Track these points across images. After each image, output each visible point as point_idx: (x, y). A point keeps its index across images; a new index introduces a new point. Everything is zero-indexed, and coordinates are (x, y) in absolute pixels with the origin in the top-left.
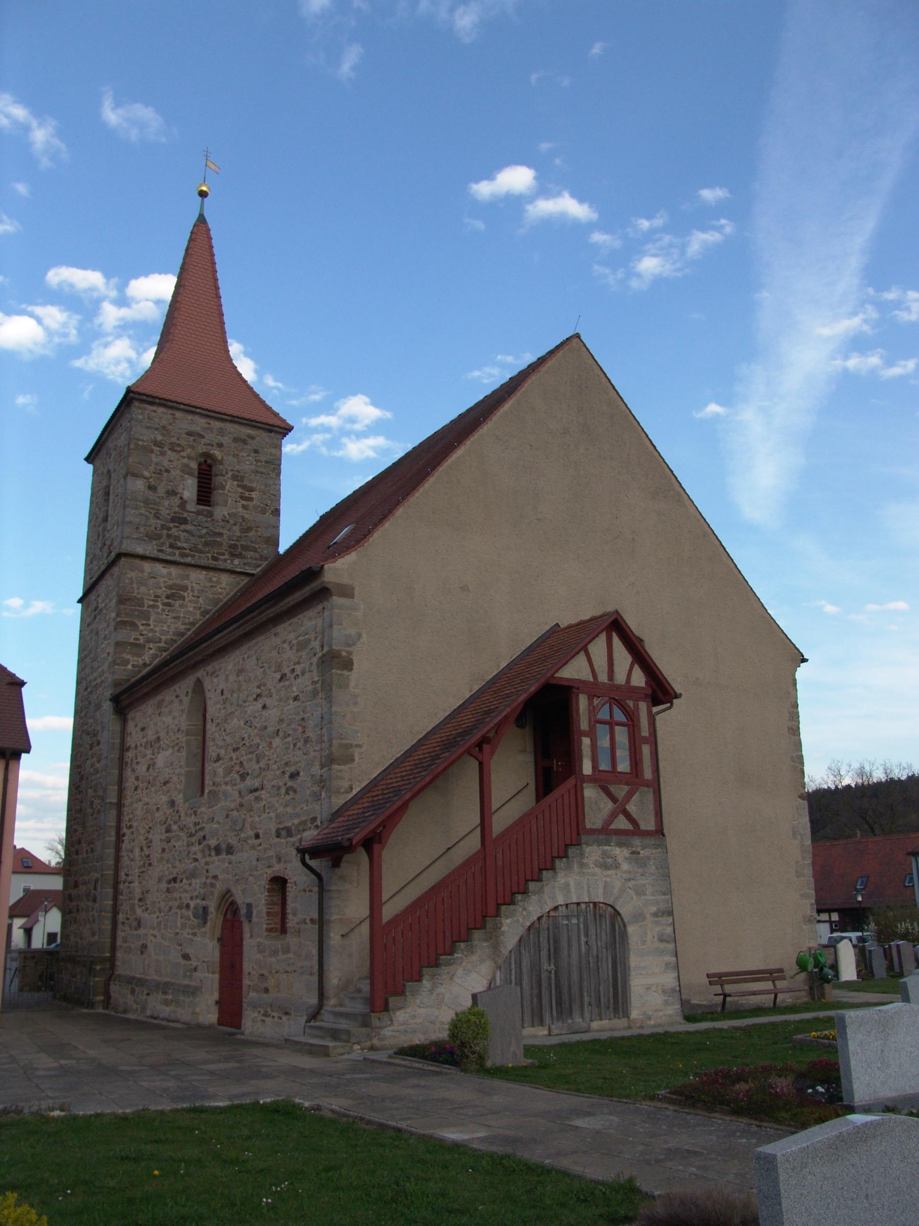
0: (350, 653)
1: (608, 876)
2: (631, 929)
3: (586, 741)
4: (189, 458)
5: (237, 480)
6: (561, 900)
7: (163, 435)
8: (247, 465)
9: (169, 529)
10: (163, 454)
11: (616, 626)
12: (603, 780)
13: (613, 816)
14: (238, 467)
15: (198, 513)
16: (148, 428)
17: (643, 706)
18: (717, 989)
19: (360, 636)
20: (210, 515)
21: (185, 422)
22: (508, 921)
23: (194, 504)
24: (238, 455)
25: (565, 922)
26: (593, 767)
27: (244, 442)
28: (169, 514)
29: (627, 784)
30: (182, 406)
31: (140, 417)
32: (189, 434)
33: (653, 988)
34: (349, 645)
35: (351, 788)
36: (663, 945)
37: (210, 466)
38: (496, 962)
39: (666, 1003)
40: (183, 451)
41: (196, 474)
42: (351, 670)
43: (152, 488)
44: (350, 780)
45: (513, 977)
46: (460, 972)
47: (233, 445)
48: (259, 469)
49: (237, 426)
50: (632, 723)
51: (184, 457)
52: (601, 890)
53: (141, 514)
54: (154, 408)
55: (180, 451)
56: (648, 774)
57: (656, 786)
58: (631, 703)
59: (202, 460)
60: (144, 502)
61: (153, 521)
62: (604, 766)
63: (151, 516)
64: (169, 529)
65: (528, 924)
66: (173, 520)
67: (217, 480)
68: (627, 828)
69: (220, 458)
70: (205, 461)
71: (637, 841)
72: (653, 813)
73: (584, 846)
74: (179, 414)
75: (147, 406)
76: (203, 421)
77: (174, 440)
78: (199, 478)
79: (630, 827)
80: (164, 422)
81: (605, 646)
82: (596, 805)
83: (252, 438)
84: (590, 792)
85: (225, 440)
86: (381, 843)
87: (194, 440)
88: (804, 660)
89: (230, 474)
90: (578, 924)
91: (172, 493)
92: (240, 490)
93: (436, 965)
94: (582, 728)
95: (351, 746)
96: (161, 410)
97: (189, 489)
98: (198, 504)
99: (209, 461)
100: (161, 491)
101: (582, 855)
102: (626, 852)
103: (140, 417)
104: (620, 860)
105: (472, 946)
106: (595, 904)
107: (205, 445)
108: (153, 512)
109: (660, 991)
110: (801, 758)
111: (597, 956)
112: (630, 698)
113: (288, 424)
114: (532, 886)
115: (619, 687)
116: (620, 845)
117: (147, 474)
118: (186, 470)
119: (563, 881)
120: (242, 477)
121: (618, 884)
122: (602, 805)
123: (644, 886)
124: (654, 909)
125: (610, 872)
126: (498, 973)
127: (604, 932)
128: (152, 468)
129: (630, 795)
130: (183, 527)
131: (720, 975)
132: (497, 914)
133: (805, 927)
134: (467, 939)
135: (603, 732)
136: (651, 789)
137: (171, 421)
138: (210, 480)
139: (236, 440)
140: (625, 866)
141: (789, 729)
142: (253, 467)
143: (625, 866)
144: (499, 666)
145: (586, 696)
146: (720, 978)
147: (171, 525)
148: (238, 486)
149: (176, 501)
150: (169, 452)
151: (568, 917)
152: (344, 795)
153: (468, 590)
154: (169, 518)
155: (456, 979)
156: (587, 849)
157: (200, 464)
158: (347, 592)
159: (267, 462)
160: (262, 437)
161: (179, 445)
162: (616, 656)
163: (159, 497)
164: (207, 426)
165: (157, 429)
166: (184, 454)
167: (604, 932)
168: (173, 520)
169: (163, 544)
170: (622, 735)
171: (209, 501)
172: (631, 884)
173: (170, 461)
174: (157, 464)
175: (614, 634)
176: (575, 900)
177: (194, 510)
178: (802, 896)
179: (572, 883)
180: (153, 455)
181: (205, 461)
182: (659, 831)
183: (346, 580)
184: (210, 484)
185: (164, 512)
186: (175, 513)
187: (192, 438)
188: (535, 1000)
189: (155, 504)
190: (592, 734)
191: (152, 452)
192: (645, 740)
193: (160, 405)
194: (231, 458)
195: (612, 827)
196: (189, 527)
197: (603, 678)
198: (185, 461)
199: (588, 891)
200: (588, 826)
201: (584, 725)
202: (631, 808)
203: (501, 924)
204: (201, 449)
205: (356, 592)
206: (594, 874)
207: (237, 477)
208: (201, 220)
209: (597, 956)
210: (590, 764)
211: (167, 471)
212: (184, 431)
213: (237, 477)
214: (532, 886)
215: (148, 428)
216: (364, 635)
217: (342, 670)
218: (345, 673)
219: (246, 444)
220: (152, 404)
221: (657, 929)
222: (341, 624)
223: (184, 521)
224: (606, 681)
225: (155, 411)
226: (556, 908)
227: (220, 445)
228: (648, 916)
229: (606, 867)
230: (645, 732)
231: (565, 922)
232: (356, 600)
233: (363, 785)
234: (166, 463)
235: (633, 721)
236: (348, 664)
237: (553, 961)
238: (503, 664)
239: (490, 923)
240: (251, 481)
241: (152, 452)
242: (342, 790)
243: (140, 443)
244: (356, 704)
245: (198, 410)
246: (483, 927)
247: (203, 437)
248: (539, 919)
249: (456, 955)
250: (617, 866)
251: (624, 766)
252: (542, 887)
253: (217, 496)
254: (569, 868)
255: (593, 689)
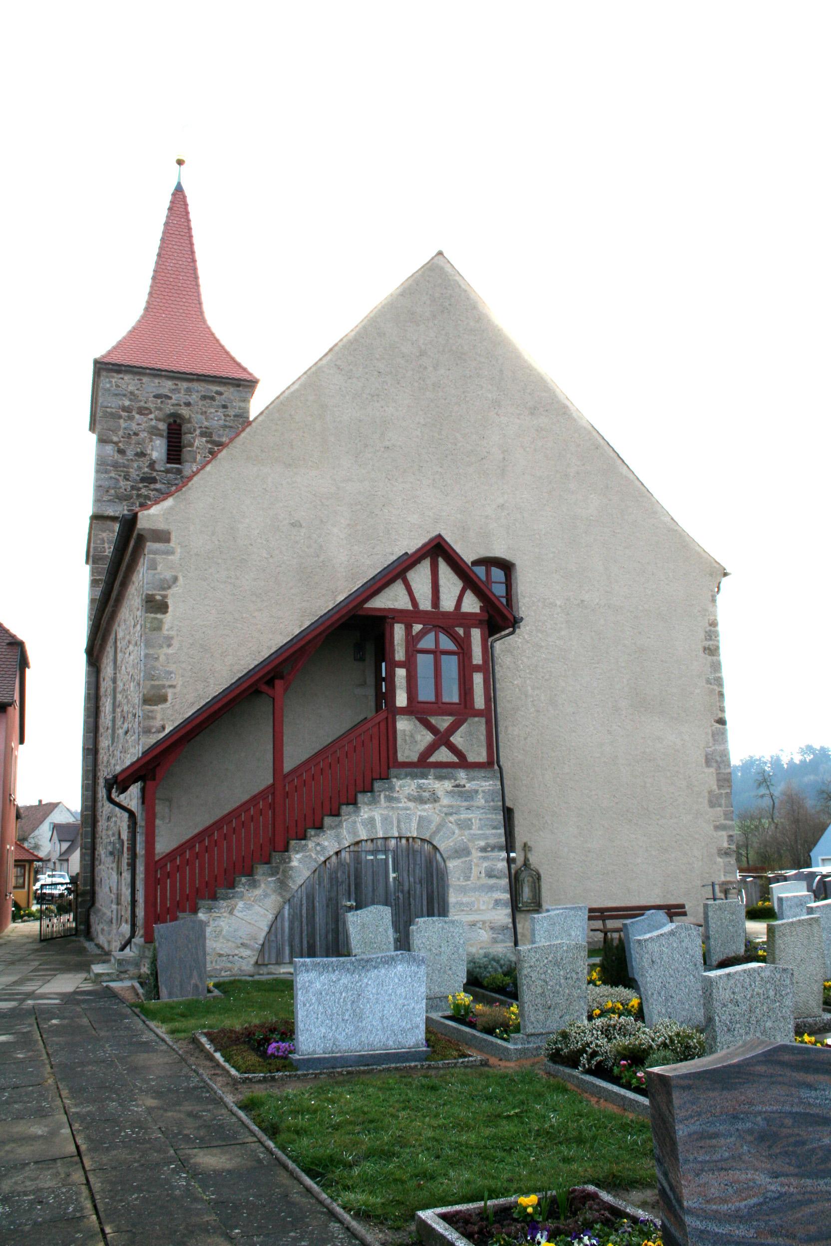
0: (165, 597)
1: (424, 810)
2: (451, 864)
3: (401, 673)
4: (157, 419)
5: (206, 437)
6: (363, 835)
7: (130, 400)
8: (216, 419)
9: (139, 489)
10: (131, 418)
11: (438, 550)
12: (415, 709)
13: (432, 749)
14: (206, 424)
15: (167, 471)
16: (116, 395)
17: (476, 634)
18: (598, 924)
19: (175, 579)
20: (179, 472)
21: (151, 386)
22: (298, 856)
23: (162, 463)
24: (206, 412)
25: (372, 857)
26: (409, 699)
27: (212, 398)
28: (138, 475)
29: (450, 714)
30: (148, 371)
31: (108, 386)
32: (157, 396)
33: (480, 925)
34: (164, 589)
35: (164, 728)
36: (492, 881)
37: (180, 426)
38: (282, 897)
39: (495, 941)
40: (151, 413)
41: (165, 434)
42: (165, 612)
43: (121, 452)
44: (163, 719)
45: (304, 911)
46: (241, 904)
47: (201, 403)
48: (227, 423)
49: (203, 384)
50: (463, 649)
51: (152, 419)
52: (414, 825)
53: (111, 478)
54: (121, 376)
55: (147, 414)
56: (479, 702)
57: (490, 715)
58: (461, 631)
59: (172, 420)
60: (113, 466)
61: (122, 483)
62: (426, 694)
63: (121, 479)
64: (139, 489)
65: (323, 859)
66: (143, 480)
67: (186, 438)
68: (449, 760)
69: (187, 417)
70: (175, 421)
71: (462, 775)
72: (484, 743)
73: (394, 780)
74: (145, 379)
75: (115, 375)
76: (169, 384)
77: (142, 404)
78: (168, 437)
79: (456, 760)
80: (131, 388)
81: (429, 573)
82: (411, 737)
83: (220, 394)
84: (403, 725)
85: (194, 398)
86: (154, 780)
87: (162, 402)
88: (725, 574)
89: (198, 432)
90: (386, 860)
91: (142, 454)
92: (210, 446)
93: (214, 897)
94: (397, 658)
95: (163, 686)
96: (127, 377)
97: (158, 450)
98: (168, 463)
99: (178, 421)
100: (130, 454)
101: (391, 789)
102: (448, 785)
103: (108, 386)
104: (440, 793)
105: (255, 881)
106: (407, 839)
107: (173, 405)
108: (123, 474)
109: (487, 928)
110: (719, 681)
111: (409, 892)
112: (460, 626)
113: (254, 377)
114: (328, 821)
115: (446, 614)
116: (440, 778)
117: (115, 439)
118: (154, 432)
119: (366, 816)
120: (211, 433)
121: (436, 819)
122: (418, 737)
123: (470, 820)
124: (482, 843)
125: (427, 806)
126: (287, 907)
127: (418, 867)
128: (121, 433)
129: (453, 728)
130: (152, 486)
131: (602, 910)
132: (286, 849)
133: (719, 860)
134: (250, 873)
135: (424, 662)
136: (483, 720)
137: (139, 386)
138: (180, 438)
139: (204, 398)
140: (445, 801)
141: (705, 649)
142: (222, 422)
143: (445, 801)
144: (335, 600)
145: (403, 626)
146: (602, 913)
147: (141, 485)
148: (207, 442)
149: (144, 463)
150: (137, 416)
151: (374, 852)
152: (155, 735)
153: (301, 526)
154: (138, 478)
155: (236, 912)
156: (397, 783)
157: (169, 425)
158: (163, 537)
159: (235, 416)
160: (229, 393)
161: (147, 409)
162: (442, 581)
163: (128, 460)
164: (174, 387)
165: (125, 395)
166: (152, 416)
167: (418, 867)
168: (143, 480)
169: (133, 504)
170: (451, 665)
171: (179, 459)
172: (452, 819)
173: (138, 424)
174: (125, 429)
175: (440, 560)
176: (381, 835)
177: (163, 469)
178: (717, 828)
179: (378, 818)
180: (122, 421)
181: (175, 421)
182: (492, 763)
183: (161, 526)
184: (180, 442)
185: (134, 473)
186: (144, 473)
187: (159, 401)
188: (330, 937)
189: (124, 467)
190: (410, 664)
191: (120, 417)
192: (478, 668)
193: (126, 372)
194: (199, 416)
195: (432, 759)
196: (158, 486)
197: (425, 605)
198: (153, 423)
199: (398, 827)
200: (401, 758)
201: (400, 655)
202: (457, 739)
203: (290, 858)
204: (169, 409)
205: (173, 537)
206: (407, 809)
207: (206, 433)
208: (179, 194)
209: (409, 892)
210: (405, 695)
211: (136, 434)
212: (152, 395)
213: (206, 433)
214: (328, 821)
215: (116, 395)
216: (181, 579)
217: (156, 613)
218: (159, 616)
219: (214, 401)
220: (119, 372)
221: (485, 864)
222: (156, 569)
223: (154, 480)
224: (429, 608)
225: (122, 379)
226: (357, 843)
227: (188, 404)
228: (473, 851)
229: (421, 800)
230: (477, 657)
231: (372, 857)
232: (172, 544)
233: (176, 725)
234: (134, 427)
235: (462, 649)
236: (161, 607)
237: (353, 896)
238: (341, 598)
239: (276, 857)
240: (220, 436)
241: (120, 417)
242: (154, 730)
243: (108, 410)
244: (169, 646)
245: (163, 373)
246: (268, 862)
247: (170, 398)
248: (337, 853)
249: (237, 889)
250: (435, 799)
251: (452, 695)
252: (341, 821)
253: (186, 452)
254: (374, 801)
255: (409, 617)
